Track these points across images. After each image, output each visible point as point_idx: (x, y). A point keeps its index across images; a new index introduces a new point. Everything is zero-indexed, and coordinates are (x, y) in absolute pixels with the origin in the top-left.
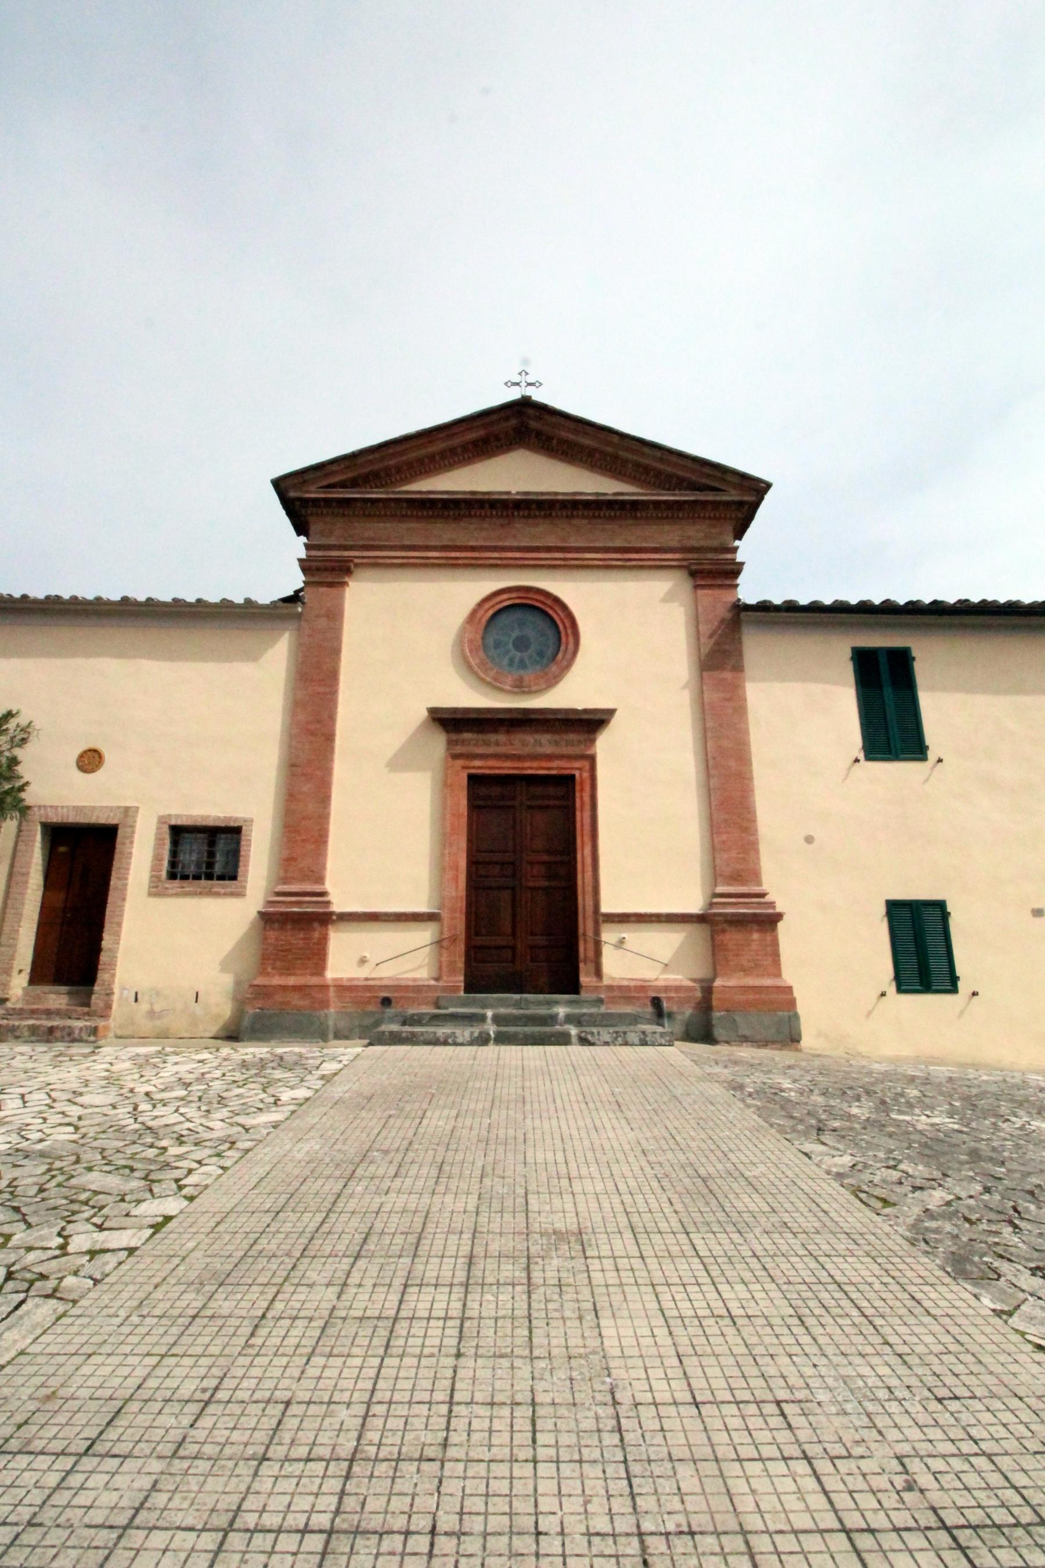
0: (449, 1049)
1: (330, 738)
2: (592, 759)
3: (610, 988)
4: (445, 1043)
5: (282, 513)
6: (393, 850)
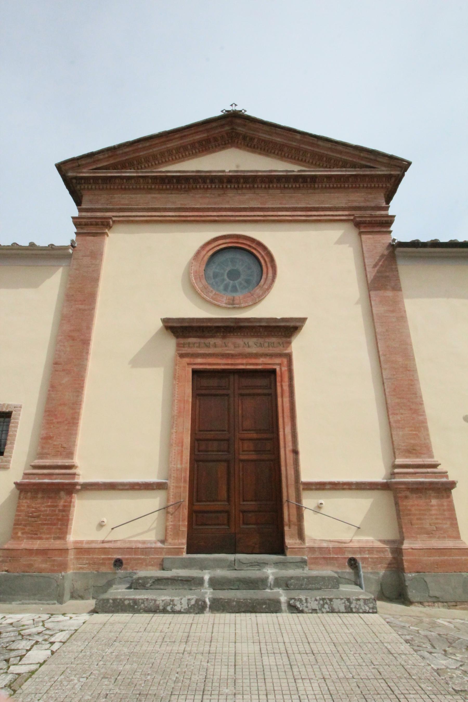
0: (167, 618)
1: (86, 342)
2: (289, 357)
3: (312, 549)
4: (164, 611)
5: (67, 192)
6: (132, 429)
